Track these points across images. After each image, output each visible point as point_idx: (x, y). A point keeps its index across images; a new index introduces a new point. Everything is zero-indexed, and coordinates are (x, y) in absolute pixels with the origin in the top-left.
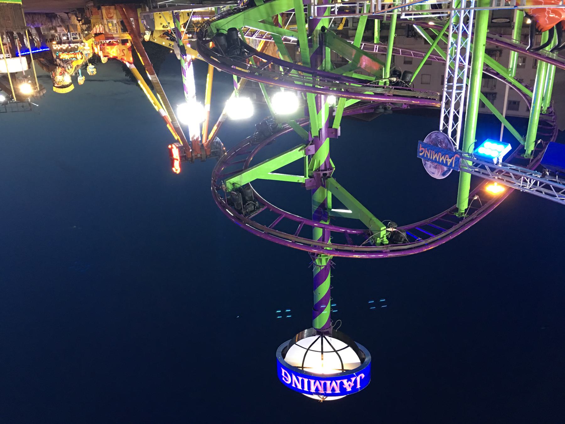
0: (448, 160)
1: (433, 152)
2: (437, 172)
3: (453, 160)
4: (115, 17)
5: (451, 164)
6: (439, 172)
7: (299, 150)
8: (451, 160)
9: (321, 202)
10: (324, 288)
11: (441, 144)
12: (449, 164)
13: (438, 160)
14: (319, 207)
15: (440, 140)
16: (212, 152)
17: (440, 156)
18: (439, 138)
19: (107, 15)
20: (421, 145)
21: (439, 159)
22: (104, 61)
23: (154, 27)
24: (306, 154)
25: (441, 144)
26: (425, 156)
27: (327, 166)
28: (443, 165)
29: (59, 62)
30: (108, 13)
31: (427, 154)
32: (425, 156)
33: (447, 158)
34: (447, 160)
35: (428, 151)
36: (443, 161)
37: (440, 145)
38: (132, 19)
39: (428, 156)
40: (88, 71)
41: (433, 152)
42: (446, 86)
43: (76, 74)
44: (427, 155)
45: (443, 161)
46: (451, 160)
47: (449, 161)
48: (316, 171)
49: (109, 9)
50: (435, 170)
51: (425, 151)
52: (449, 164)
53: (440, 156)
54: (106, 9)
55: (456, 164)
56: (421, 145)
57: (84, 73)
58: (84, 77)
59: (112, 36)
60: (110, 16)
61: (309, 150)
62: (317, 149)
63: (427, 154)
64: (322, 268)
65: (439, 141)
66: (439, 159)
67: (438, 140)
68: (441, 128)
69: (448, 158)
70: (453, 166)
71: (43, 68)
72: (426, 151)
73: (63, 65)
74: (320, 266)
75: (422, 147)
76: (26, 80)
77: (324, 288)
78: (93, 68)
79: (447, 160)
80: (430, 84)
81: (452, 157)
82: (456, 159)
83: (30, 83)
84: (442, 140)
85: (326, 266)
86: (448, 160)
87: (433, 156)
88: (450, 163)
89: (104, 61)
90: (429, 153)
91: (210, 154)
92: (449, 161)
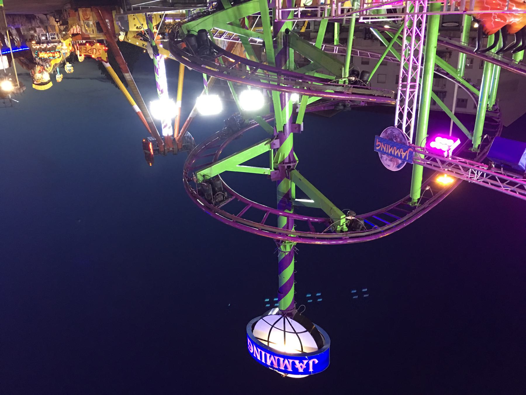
0: (403, 153)
1: (389, 146)
2: (392, 165)
3: (407, 153)
4: (91, 18)
5: (405, 157)
6: (394, 164)
7: (265, 144)
8: (405, 154)
9: (286, 192)
10: (289, 272)
11: (396, 139)
12: (403, 157)
13: (393, 153)
14: (284, 197)
15: (395, 135)
16: (183, 146)
17: (395, 150)
18: (394, 133)
19: (84, 17)
20: (377, 139)
21: (394, 152)
22: (80, 60)
23: (129, 29)
24: (271, 147)
25: (396, 139)
26: (382, 150)
27: (291, 159)
28: (397, 158)
29: (38, 61)
30: (85, 15)
31: (383, 148)
32: (382, 150)
33: (401, 152)
34: (401, 153)
35: (384, 146)
36: (397, 154)
37: (395, 140)
38: (107, 20)
39: (384, 150)
40: (65, 69)
41: (389, 146)
42: (400, 85)
43: (54, 72)
44: (383, 149)
45: (397, 154)
46: (405, 154)
47: (404, 154)
48: (280, 163)
49: (86, 11)
50: (390, 162)
51: (381, 145)
52: (403, 157)
53: (395, 150)
54: (83, 12)
55: (410, 157)
56: (377, 139)
57: (62, 71)
58: (62, 75)
59: (88, 36)
60: (86, 17)
61: (274, 144)
62: (281, 143)
63: (383, 148)
64: (287, 253)
65: (394, 136)
66: (394, 152)
67: (393, 135)
68: (396, 123)
69: (402, 151)
70: (407, 159)
71: (23, 66)
72: (383, 145)
73: (42, 64)
74: (285, 252)
75: (378, 142)
76: (7, 78)
77: (289, 272)
78: (70, 67)
79: (401, 153)
80: (385, 83)
81: (406, 150)
82: (409, 153)
83: (11, 81)
84: (397, 135)
85: (290, 252)
86: (403, 153)
87: (388, 150)
88: (404, 156)
89: (80, 60)
90: (385, 147)
91: (182, 148)
92: (403, 155)
